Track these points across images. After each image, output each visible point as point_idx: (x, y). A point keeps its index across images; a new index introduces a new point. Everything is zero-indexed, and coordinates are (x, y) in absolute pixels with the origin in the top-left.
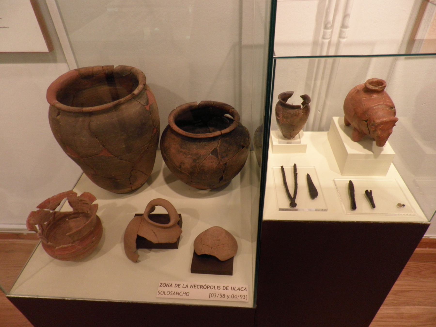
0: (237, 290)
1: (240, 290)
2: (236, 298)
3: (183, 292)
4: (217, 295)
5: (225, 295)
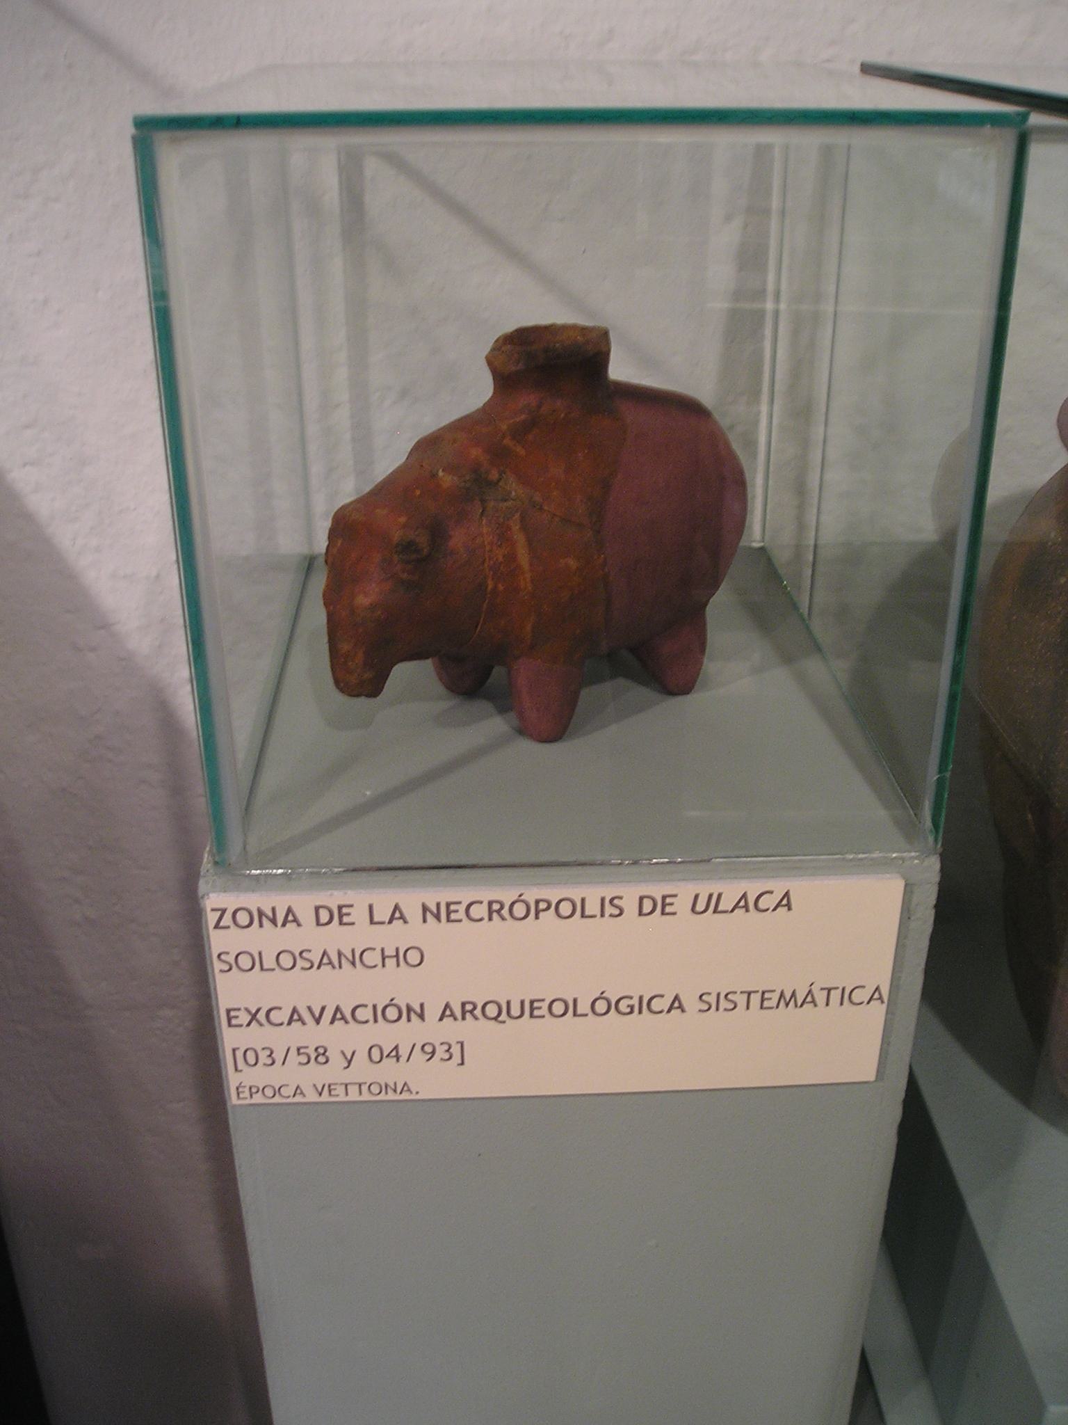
0: (732, 911)
1: (747, 911)
2: (398, 1060)
3: (383, 950)
4: (279, 1056)
5: (325, 1051)
